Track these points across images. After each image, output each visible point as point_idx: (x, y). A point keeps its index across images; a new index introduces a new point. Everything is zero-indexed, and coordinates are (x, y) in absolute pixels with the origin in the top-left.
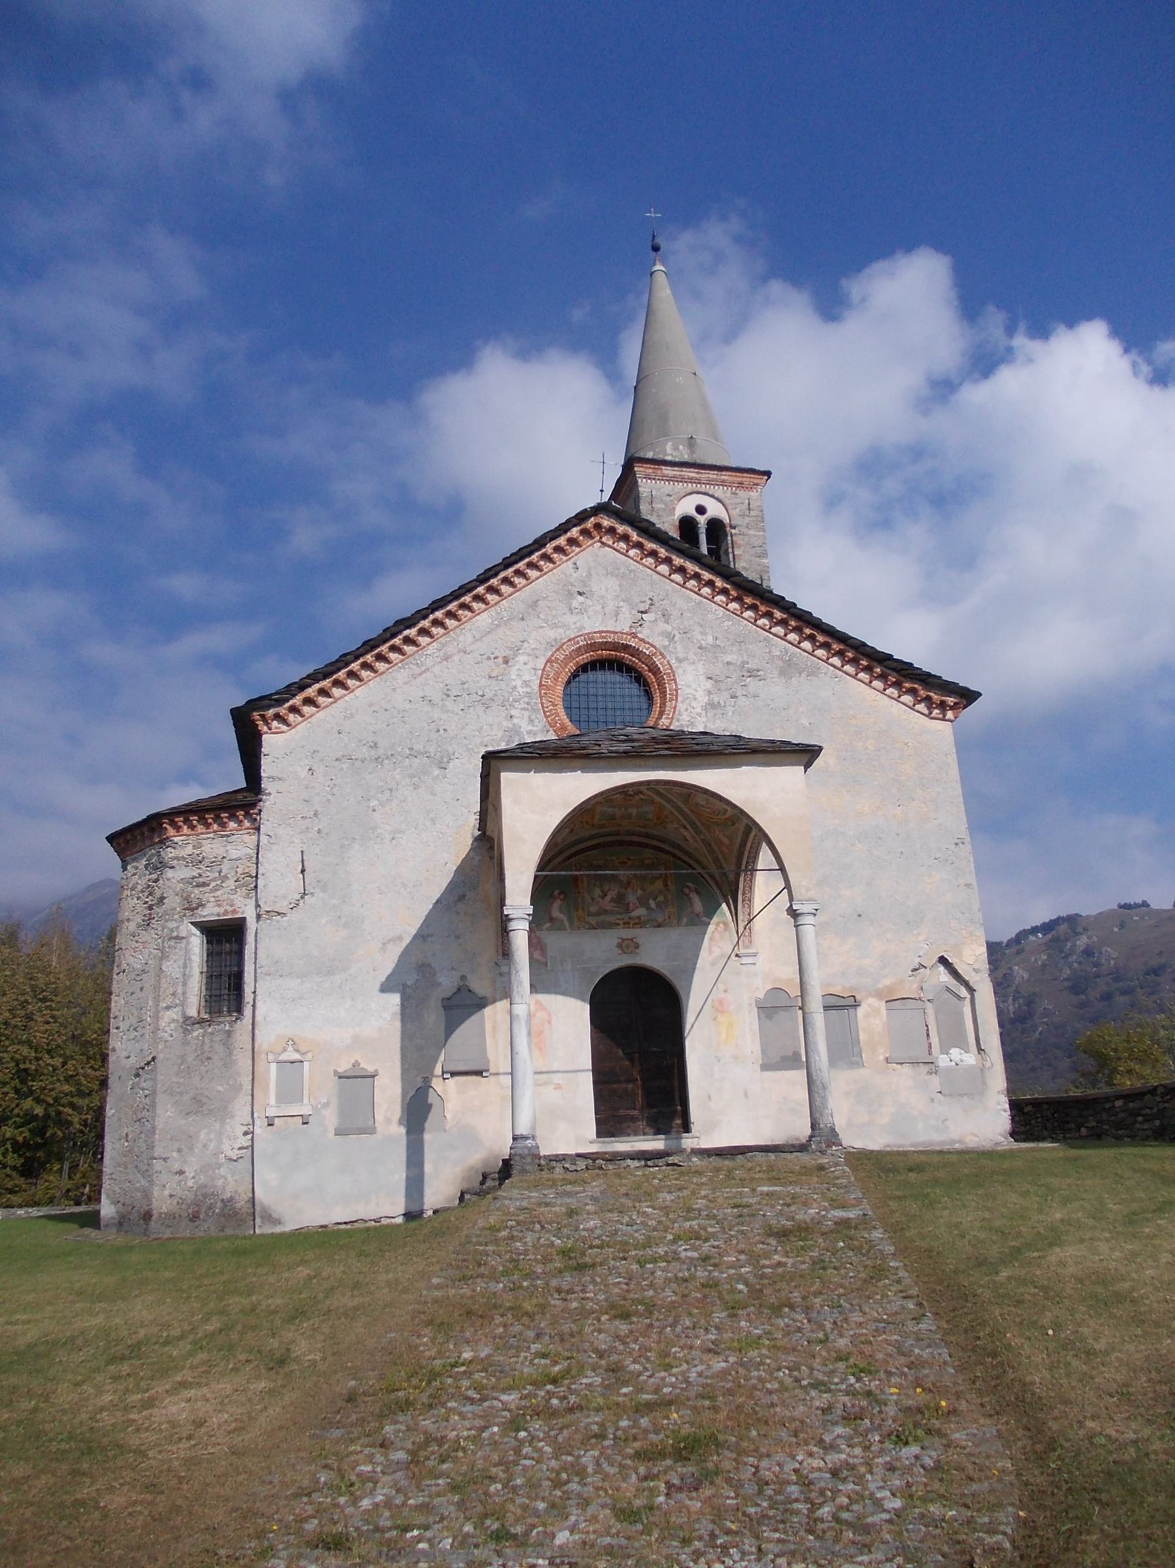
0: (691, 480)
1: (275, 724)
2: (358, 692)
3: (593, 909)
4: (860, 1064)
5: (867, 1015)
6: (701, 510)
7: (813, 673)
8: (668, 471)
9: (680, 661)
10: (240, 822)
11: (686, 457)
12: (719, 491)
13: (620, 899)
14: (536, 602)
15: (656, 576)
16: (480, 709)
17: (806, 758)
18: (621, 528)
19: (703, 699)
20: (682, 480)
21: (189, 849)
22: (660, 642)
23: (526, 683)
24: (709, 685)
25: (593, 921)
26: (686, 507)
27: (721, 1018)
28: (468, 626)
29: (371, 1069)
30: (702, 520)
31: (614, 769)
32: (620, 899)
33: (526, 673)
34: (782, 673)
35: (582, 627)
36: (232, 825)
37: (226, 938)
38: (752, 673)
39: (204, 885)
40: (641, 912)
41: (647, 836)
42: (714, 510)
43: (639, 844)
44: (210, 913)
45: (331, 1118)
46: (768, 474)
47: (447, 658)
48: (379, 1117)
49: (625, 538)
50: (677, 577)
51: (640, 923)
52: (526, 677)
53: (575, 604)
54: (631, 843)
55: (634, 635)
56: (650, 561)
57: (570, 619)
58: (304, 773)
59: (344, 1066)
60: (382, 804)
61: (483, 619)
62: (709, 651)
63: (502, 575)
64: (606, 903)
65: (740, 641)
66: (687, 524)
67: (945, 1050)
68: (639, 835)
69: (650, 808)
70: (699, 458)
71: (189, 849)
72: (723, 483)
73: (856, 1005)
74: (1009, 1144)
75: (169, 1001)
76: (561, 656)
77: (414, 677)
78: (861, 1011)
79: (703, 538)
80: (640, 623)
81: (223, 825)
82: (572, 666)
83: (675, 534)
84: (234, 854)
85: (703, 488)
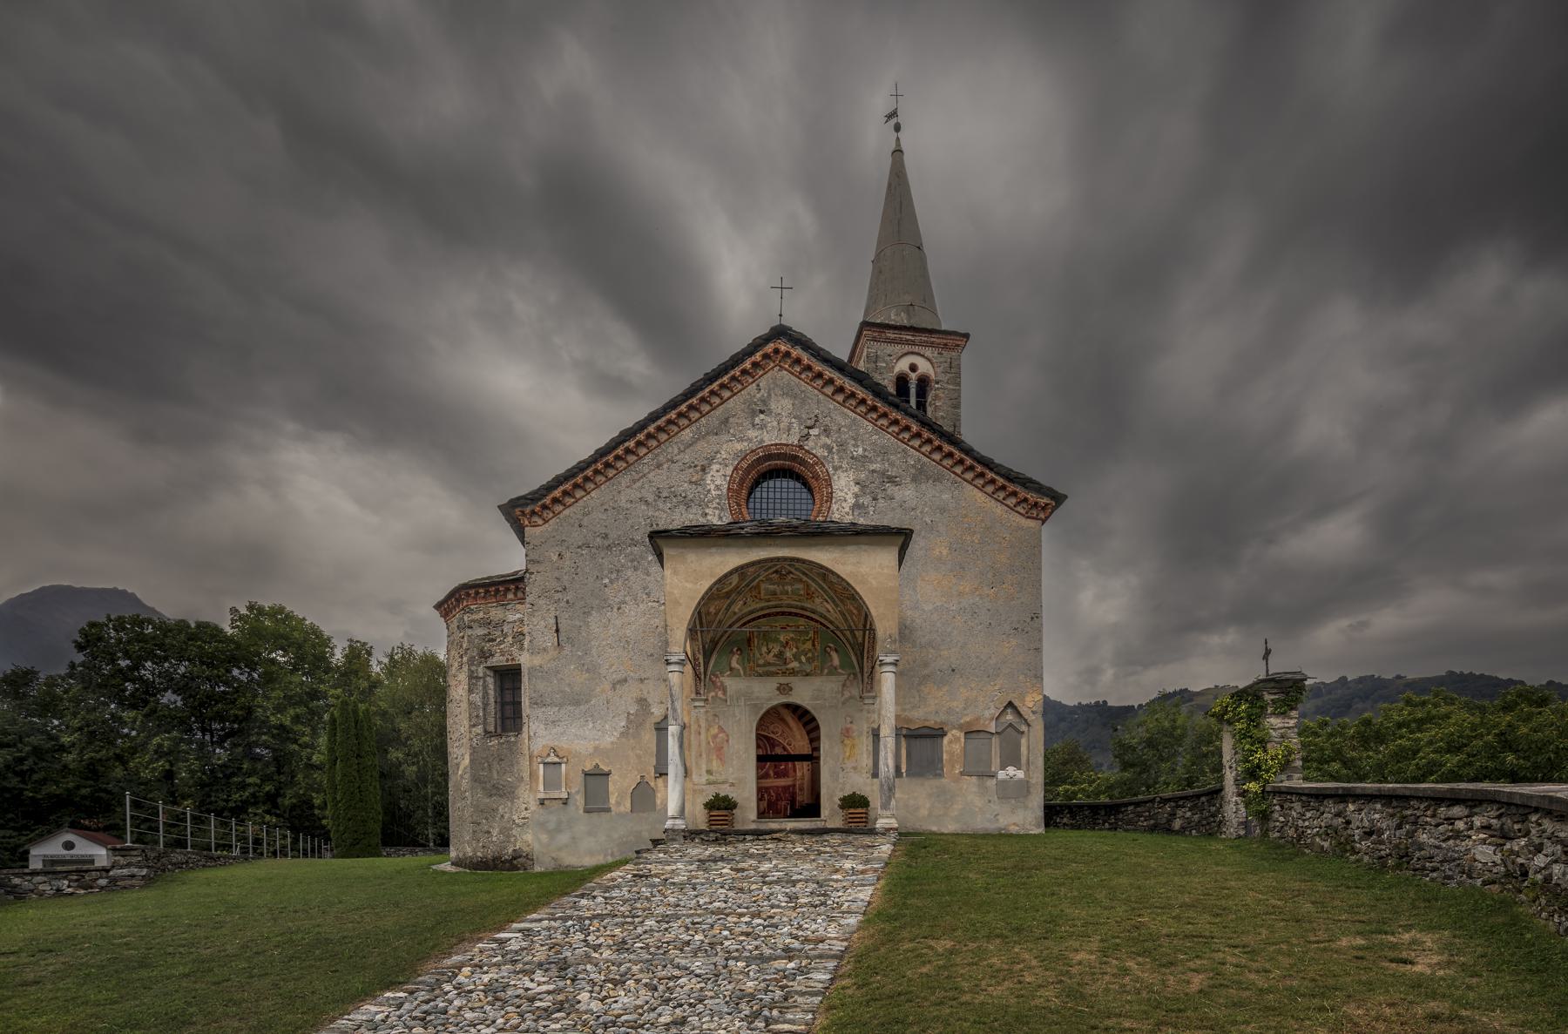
0: (907, 342)
3: (761, 662)
4: (941, 776)
5: (950, 742)
6: (913, 368)
7: (938, 479)
8: (891, 334)
9: (836, 469)
11: (905, 323)
12: (928, 352)
14: (727, 420)
15: (821, 397)
17: (901, 540)
19: (851, 501)
21: (481, 615)
22: (820, 452)
23: (718, 488)
24: (856, 489)
25: (760, 670)
26: (903, 366)
27: (847, 742)
28: (675, 439)
29: (606, 769)
30: (913, 376)
31: (758, 546)
33: (718, 479)
34: (914, 479)
35: (762, 441)
38: (892, 480)
41: (803, 608)
42: (924, 367)
43: (796, 615)
45: (579, 800)
46: (967, 336)
47: (659, 466)
48: (613, 800)
51: (793, 673)
52: (718, 482)
53: (757, 420)
54: (790, 614)
55: (801, 447)
57: (752, 433)
58: (555, 558)
59: (588, 767)
60: (611, 582)
63: (700, 395)
65: (884, 452)
66: (902, 381)
67: (1003, 768)
68: (821, 615)
69: (801, 586)
70: (915, 322)
71: (481, 615)
72: (932, 345)
73: (944, 735)
74: (1041, 830)
76: (744, 465)
77: (634, 481)
78: (946, 740)
79: (913, 391)
82: (753, 474)
83: (892, 389)
84: (511, 618)
85: (916, 349)
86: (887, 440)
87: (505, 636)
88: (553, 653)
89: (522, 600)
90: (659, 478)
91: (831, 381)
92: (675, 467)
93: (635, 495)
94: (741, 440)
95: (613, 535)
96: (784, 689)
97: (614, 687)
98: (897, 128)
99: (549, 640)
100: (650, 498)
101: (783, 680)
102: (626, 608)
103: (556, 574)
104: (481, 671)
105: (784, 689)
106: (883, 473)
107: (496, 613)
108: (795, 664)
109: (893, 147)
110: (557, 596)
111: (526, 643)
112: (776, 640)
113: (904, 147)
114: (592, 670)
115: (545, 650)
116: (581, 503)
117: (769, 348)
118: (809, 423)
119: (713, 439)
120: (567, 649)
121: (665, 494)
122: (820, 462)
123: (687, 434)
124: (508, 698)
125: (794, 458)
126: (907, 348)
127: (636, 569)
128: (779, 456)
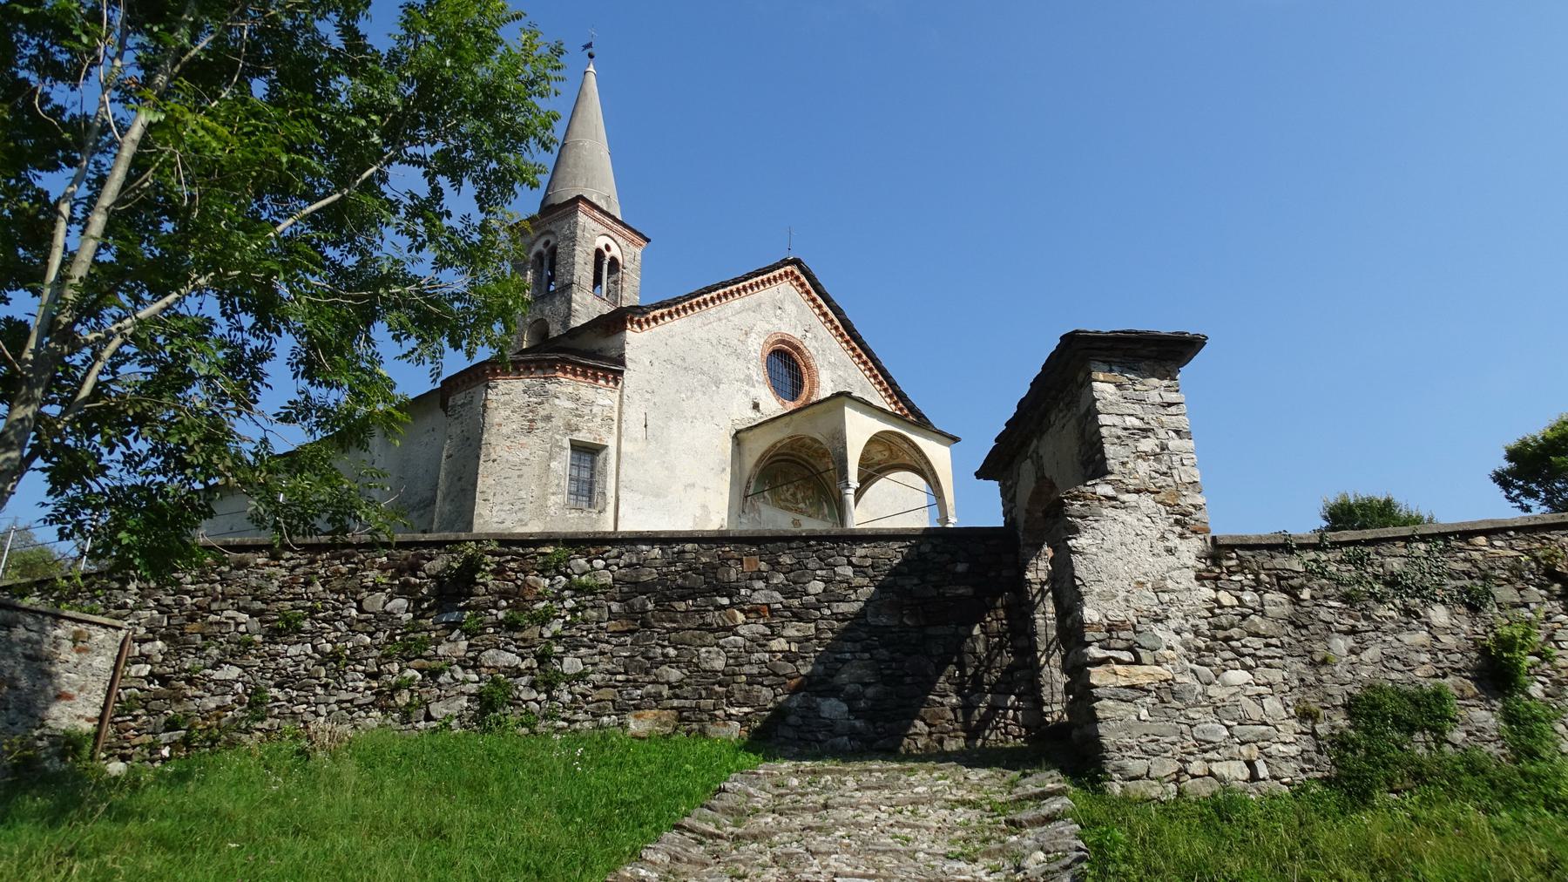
0: (607, 226)
6: (608, 247)
8: (597, 214)
12: (620, 240)
13: (794, 495)
18: (803, 279)
20: (602, 223)
30: (608, 255)
32: (794, 495)
36: (602, 382)
37: (588, 452)
40: (802, 505)
42: (615, 252)
44: (583, 436)
49: (802, 285)
51: (802, 512)
57: (775, 321)
61: (736, 303)
62: (833, 366)
64: (788, 495)
71: (570, 389)
72: (623, 236)
75: (554, 489)
81: (596, 380)
84: (601, 402)
87: (595, 416)
91: (820, 307)
95: (689, 360)
101: (798, 516)
102: (697, 423)
104: (567, 444)
110: (648, 396)
117: (789, 268)
120: (653, 445)
125: (797, 348)
126: (606, 231)
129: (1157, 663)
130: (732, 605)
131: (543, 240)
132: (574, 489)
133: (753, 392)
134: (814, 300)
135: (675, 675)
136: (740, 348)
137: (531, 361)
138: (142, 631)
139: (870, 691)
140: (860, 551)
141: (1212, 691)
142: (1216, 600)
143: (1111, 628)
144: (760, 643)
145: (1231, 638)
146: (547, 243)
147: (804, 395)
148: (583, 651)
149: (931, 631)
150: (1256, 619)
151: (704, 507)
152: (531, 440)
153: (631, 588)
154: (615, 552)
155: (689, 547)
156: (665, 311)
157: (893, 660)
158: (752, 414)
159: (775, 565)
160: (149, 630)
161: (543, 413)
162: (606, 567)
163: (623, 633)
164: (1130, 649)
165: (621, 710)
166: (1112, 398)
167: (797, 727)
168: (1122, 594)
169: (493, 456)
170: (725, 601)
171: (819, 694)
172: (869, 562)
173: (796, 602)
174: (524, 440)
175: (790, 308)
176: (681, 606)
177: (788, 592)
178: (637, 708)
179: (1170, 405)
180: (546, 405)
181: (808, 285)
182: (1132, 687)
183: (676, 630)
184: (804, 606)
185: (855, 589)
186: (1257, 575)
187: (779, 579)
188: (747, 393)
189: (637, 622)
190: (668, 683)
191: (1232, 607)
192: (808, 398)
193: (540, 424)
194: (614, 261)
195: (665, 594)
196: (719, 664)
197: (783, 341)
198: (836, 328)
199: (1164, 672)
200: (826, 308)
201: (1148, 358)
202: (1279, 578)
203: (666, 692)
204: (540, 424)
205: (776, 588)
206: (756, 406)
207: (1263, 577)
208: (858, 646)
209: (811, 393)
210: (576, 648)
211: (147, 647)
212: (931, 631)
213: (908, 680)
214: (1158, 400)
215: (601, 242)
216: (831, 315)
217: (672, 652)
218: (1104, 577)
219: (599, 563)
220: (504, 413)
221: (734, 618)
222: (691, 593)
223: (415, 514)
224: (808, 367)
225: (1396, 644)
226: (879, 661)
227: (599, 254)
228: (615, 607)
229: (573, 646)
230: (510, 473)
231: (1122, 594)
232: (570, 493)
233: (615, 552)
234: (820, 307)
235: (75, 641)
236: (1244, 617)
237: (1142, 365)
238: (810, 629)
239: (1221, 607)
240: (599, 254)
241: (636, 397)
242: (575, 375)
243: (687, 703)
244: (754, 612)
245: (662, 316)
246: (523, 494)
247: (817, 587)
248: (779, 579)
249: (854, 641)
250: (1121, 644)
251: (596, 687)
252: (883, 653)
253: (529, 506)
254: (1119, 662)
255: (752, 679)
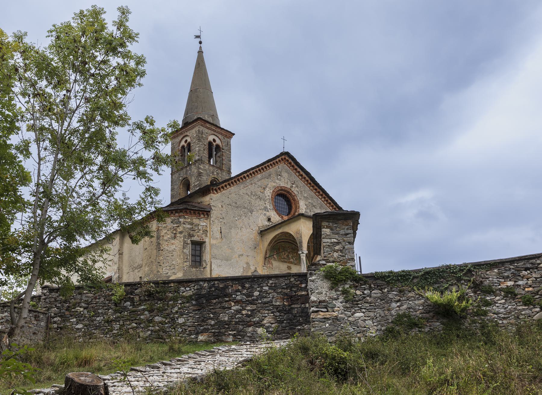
1: (214, 191)
2: (232, 188)
6: (214, 140)
8: (208, 125)
10: (204, 216)
11: (212, 122)
12: (220, 136)
13: (288, 256)
16: (259, 200)
21: (189, 220)
23: (268, 196)
24: (305, 207)
25: (282, 260)
30: (214, 144)
32: (288, 256)
36: (202, 216)
38: (314, 206)
39: (194, 231)
40: (292, 260)
42: (218, 142)
44: (196, 238)
46: (234, 134)
49: (290, 163)
50: (300, 177)
51: (291, 263)
56: (295, 171)
57: (277, 181)
58: (220, 207)
62: (306, 198)
71: (189, 220)
72: (221, 134)
80: (292, 187)
84: (202, 224)
86: (313, 194)
87: (200, 230)
88: (219, 240)
89: (207, 219)
90: (252, 188)
91: (299, 172)
92: (256, 186)
93: (245, 192)
94: (274, 182)
95: (238, 203)
96: (289, 268)
97: (239, 257)
98: (200, 43)
99: (218, 235)
100: (249, 194)
101: (289, 265)
102: (243, 229)
103: (221, 212)
104: (189, 241)
105: (289, 268)
106: (312, 204)
107: (196, 221)
108: (292, 260)
109: (198, 49)
110: (221, 220)
111: (208, 234)
112: (287, 251)
113: (203, 50)
114: (232, 249)
115: (217, 238)
116: (228, 190)
117: (283, 157)
118: (293, 183)
119: (266, 180)
120: (224, 240)
121: (253, 194)
122: (295, 195)
123: (259, 176)
124: (198, 253)
125: (288, 192)
126: (213, 132)
127: (246, 217)
128: (284, 190)
129: (333, 311)
130: (230, 300)
131: (184, 140)
132: (193, 259)
133: (268, 214)
134: (296, 169)
135: (213, 322)
136: (261, 195)
137: (173, 210)
138: (53, 315)
139: (273, 325)
140: (271, 282)
141: (350, 319)
142: (355, 293)
143: (320, 302)
144: (238, 312)
145: (359, 304)
146: (186, 141)
147: (292, 213)
148: (185, 316)
149: (293, 306)
150: (368, 298)
151: (247, 263)
152: (176, 242)
153: (198, 297)
154: (193, 285)
155: (216, 282)
156: (227, 183)
157: (280, 316)
158: (267, 223)
159: (244, 287)
160: (55, 314)
161: (179, 230)
162: (190, 290)
163: (196, 310)
164: (326, 308)
165: (197, 334)
166: (328, 233)
167: (250, 337)
168: (324, 293)
169: (162, 248)
170: (227, 299)
171: (257, 327)
172: (274, 285)
173: (250, 299)
174: (173, 241)
175: (285, 175)
176: (215, 301)
177: (248, 296)
178: (201, 332)
179: (348, 234)
180: (180, 227)
181: (293, 163)
182: (325, 318)
183: (213, 309)
184: (253, 300)
185: (269, 294)
186: (370, 285)
187: (245, 291)
188: (265, 214)
189: (200, 307)
190: (211, 325)
191: (361, 295)
192: (294, 214)
193: (178, 235)
194: (218, 146)
195: (209, 297)
196: (226, 319)
197: (282, 190)
198: (307, 181)
199: (335, 314)
200: (302, 173)
201: (342, 219)
202: (378, 286)
203: (209, 327)
204: (178, 235)
205: (244, 294)
206: (269, 220)
207: (372, 286)
208: (270, 312)
209: (296, 211)
210: (182, 315)
211: (55, 319)
212: (293, 306)
213: (285, 322)
214: (344, 233)
215: (211, 138)
216: (304, 175)
217: (212, 316)
218: (319, 288)
219: (188, 289)
220: (164, 231)
221: (231, 304)
222: (218, 297)
223: (137, 271)
224: (294, 200)
225: (413, 304)
226: (276, 316)
227: (210, 144)
228: (194, 302)
229: (182, 315)
230: (169, 255)
231: (324, 293)
232: (192, 261)
233: (193, 285)
234: (299, 172)
235: (35, 318)
236: (364, 298)
237: (340, 222)
238: (255, 307)
239: (356, 295)
240: (210, 144)
241: (216, 221)
242: (191, 214)
243: (217, 331)
244: (237, 302)
245: (226, 186)
246: (174, 262)
247: (256, 293)
248: (245, 291)
249: (268, 310)
250: (322, 306)
251: (189, 327)
252: (278, 314)
253: (177, 267)
254: (322, 311)
255: (237, 323)
